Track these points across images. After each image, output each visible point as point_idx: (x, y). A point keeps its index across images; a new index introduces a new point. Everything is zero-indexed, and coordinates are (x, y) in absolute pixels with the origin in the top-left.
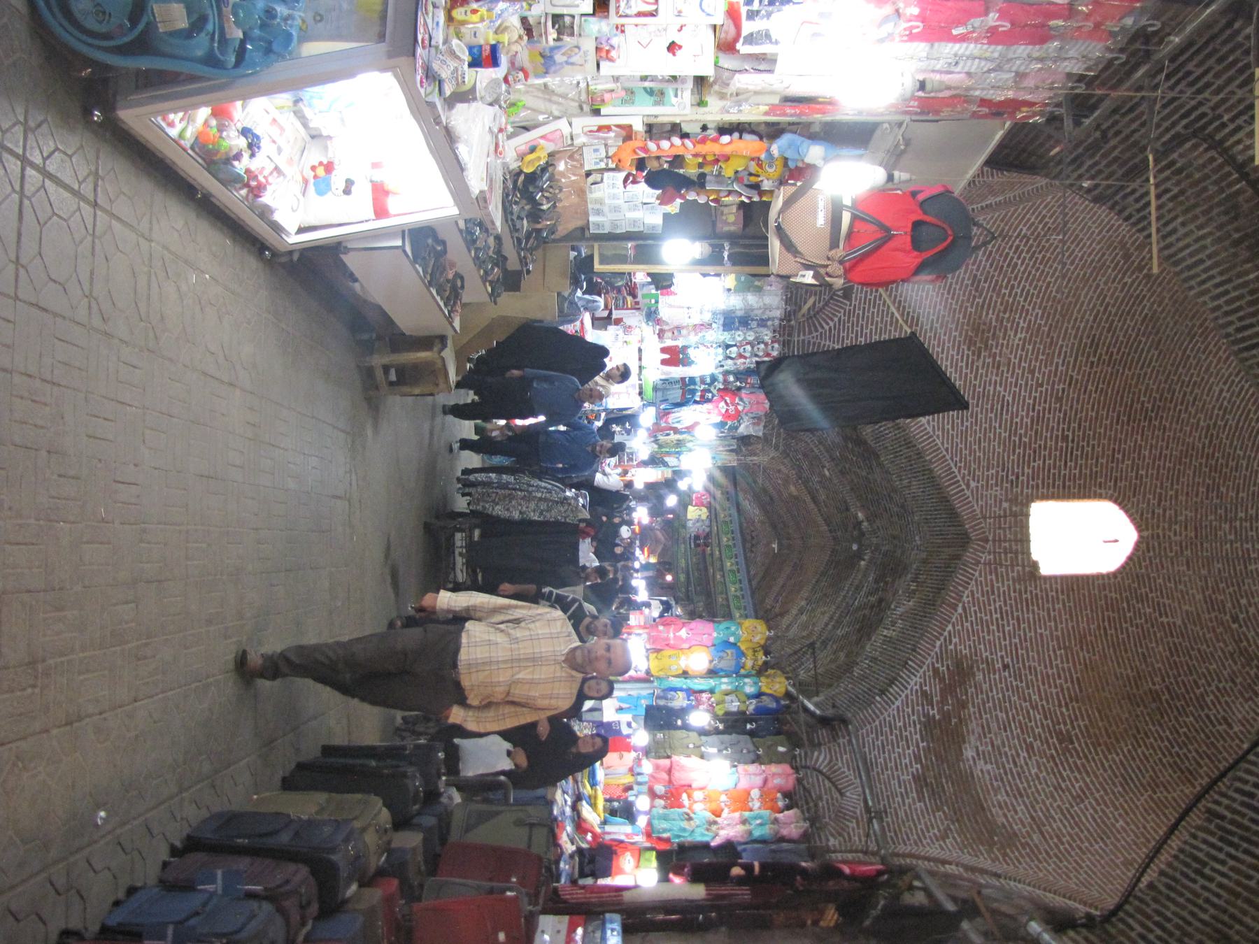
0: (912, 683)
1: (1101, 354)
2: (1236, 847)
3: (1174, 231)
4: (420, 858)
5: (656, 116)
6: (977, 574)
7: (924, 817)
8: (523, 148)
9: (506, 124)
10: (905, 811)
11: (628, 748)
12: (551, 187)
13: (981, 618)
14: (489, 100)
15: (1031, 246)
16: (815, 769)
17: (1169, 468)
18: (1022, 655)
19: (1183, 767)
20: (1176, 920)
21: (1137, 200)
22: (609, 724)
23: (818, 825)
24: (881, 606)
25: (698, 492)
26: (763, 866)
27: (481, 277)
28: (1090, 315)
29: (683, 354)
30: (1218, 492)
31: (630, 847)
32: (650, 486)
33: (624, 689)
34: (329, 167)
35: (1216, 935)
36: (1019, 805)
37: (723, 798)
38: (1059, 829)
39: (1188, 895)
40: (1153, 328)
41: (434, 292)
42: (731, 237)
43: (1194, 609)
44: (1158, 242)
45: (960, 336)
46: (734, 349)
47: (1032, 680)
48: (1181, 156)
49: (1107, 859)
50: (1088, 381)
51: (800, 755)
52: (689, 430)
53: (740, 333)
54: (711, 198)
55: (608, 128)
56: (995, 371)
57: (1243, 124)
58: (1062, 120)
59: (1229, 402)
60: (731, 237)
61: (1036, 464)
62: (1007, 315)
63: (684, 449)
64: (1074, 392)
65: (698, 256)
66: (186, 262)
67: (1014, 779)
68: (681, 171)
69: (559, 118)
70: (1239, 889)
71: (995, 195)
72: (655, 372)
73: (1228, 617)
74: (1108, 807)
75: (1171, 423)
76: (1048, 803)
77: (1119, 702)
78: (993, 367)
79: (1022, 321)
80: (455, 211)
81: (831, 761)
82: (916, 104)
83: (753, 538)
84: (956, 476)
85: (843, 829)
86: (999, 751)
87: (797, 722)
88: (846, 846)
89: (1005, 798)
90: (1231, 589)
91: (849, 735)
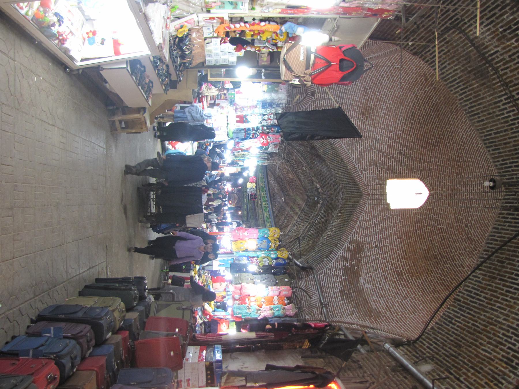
0: (339, 253)
1: (416, 120)
2: (464, 312)
3: (445, 67)
4: (138, 323)
5: (234, 14)
6: (365, 209)
7: (344, 307)
8: (178, 26)
9: (171, 15)
10: (336, 304)
11: (223, 281)
12: (190, 44)
13: (367, 226)
14: (163, 2)
15: (388, 75)
16: (300, 288)
17: (442, 166)
18: (383, 241)
19: (445, 284)
20: (441, 340)
21: (431, 54)
22: (216, 271)
23: (301, 310)
24: (326, 223)
25: (252, 177)
26: (278, 324)
27: (160, 82)
28: (411, 104)
29: (245, 118)
30: (461, 175)
31: (225, 321)
32: (232, 175)
33: (221, 257)
34: (94, 33)
35: (456, 345)
36: (382, 301)
37: (263, 300)
38: (397, 309)
39: (446, 331)
40: (436, 109)
41: (140, 88)
42: (265, 67)
43: (451, 222)
44: (439, 72)
45: (359, 112)
46: (266, 116)
47: (387, 251)
48: (448, 36)
49: (416, 320)
50: (410, 130)
51: (294, 282)
52: (248, 150)
53: (269, 109)
54: (257, 49)
55: (214, 18)
56: (373, 126)
57: (473, 23)
58: (401, 18)
59: (466, 139)
60: (265, 67)
61: (389, 164)
62: (378, 103)
63: (245, 158)
64: (405, 135)
65: (251, 74)
66: (32, 71)
67: (380, 291)
68: (244, 38)
69: (193, 14)
70: (465, 327)
71: (374, 54)
72: (234, 126)
73: (464, 225)
74: (416, 301)
75: (443, 148)
76: (393, 299)
77: (421, 259)
78: (372, 125)
79: (384, 106)
80: (149, 53)
81: (306, 285)
82: (342, 10)
83: (274, 196)
84: (357, 169)
85: (311, 312)
86: (374, 280)
87: (293, 269)
88: (313, 319)
89: (376, 298)
90: (465, 214)
91: (314, 274)
